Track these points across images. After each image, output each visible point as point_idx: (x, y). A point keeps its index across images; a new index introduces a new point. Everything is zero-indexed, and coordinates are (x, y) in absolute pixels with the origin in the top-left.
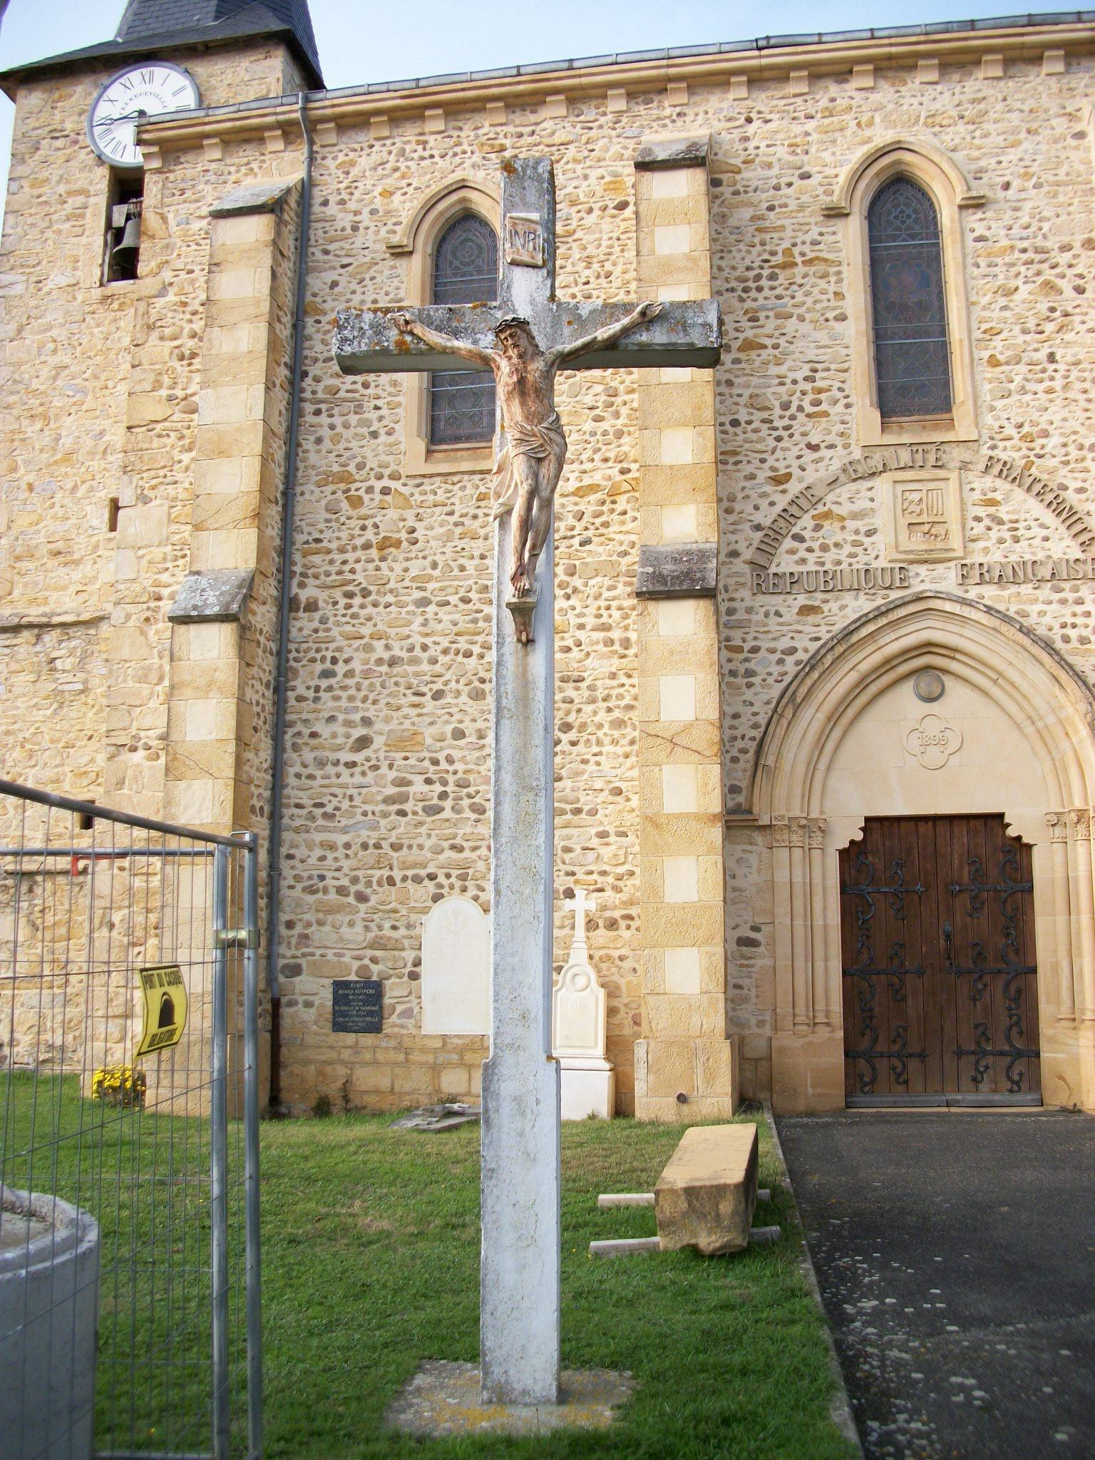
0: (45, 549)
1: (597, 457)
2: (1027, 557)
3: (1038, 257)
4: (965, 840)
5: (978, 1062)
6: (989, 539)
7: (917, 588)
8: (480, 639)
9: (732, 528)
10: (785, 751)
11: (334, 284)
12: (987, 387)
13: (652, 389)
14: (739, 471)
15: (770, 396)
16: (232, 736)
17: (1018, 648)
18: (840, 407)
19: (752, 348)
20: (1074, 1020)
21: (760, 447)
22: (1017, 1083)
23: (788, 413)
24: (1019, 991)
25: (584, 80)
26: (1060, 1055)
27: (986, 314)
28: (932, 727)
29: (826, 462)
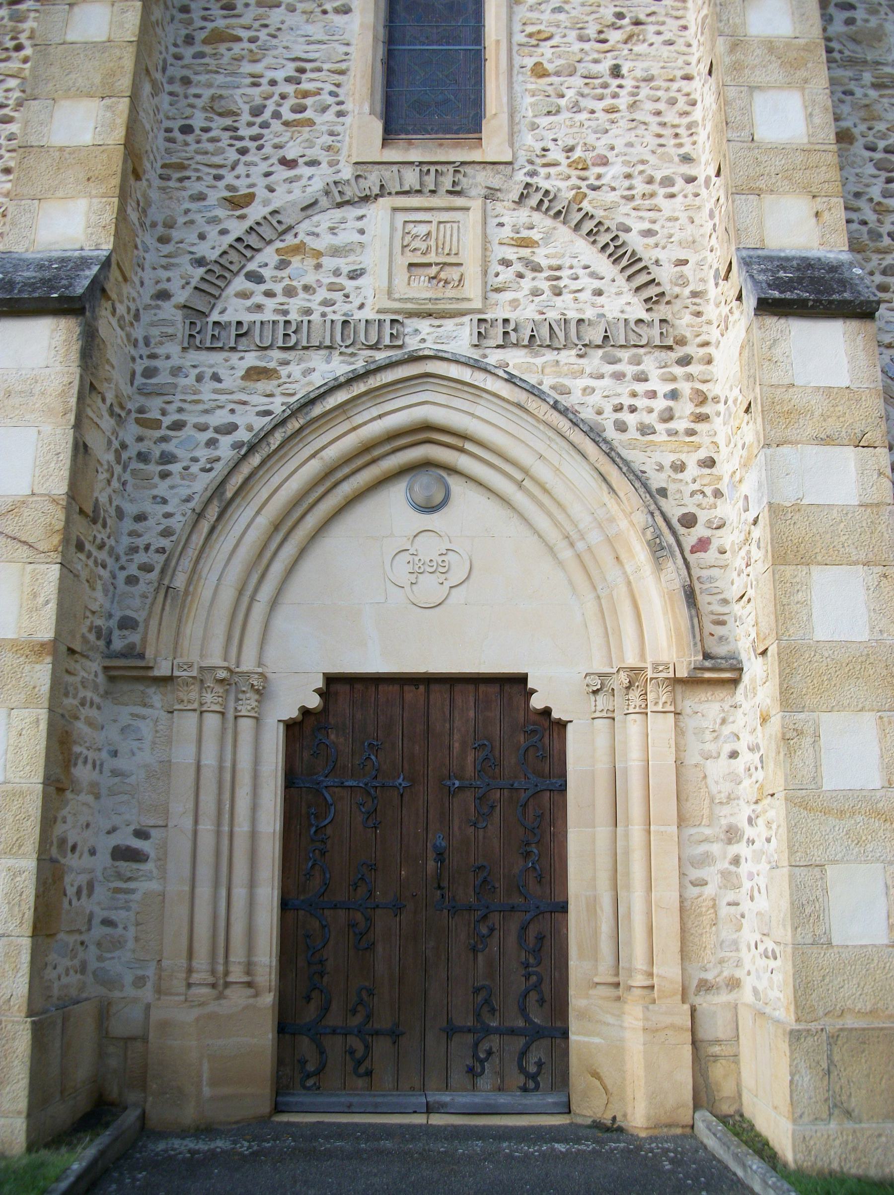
2: (573, 315)
4: (472, 714)
5: (476, 1045)
6: (520, 288)
7: (412, 344)
9: (164, 261)
10: (205, 567)
12: (529, 100)
13: (51, 50)
14: (184, 189)
15: (237, 98)
17: (551, 433)
18: (330, 116)
19: (223, 41)
20: (617, 985)
21: (217, 160)
22: (534, 1077)
23: (259, 120)
24: (541, 938)
26: (597, 1040)
28: (428, 548)
29: (304, 182)
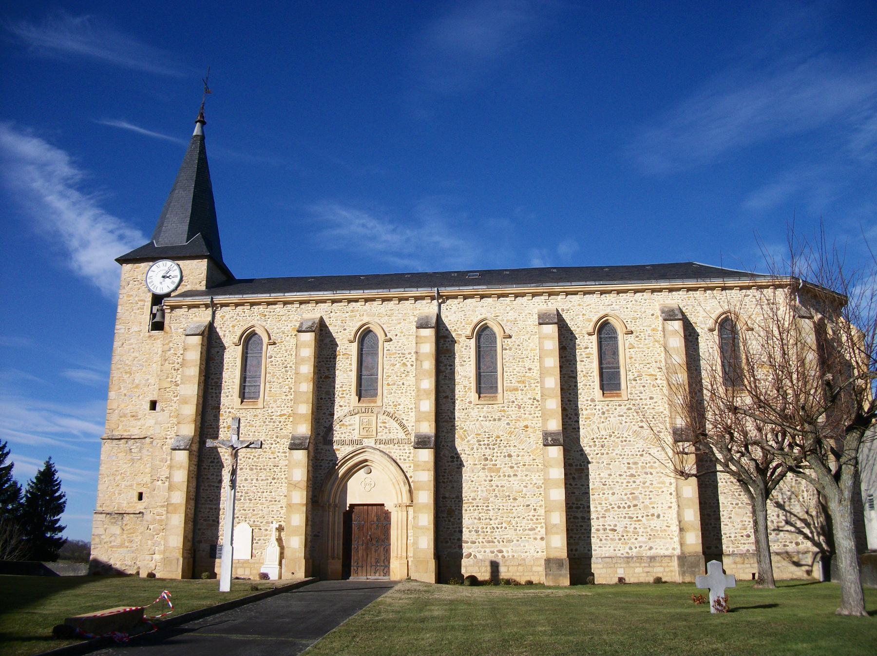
0: (129, 415)
1: (286, 406)
3: (402, 356)
8: (253, 454)
11: (218, 352)
12: (386, 391)
16: (186, 480)
25: (288, 299)
27: (388, 371)
